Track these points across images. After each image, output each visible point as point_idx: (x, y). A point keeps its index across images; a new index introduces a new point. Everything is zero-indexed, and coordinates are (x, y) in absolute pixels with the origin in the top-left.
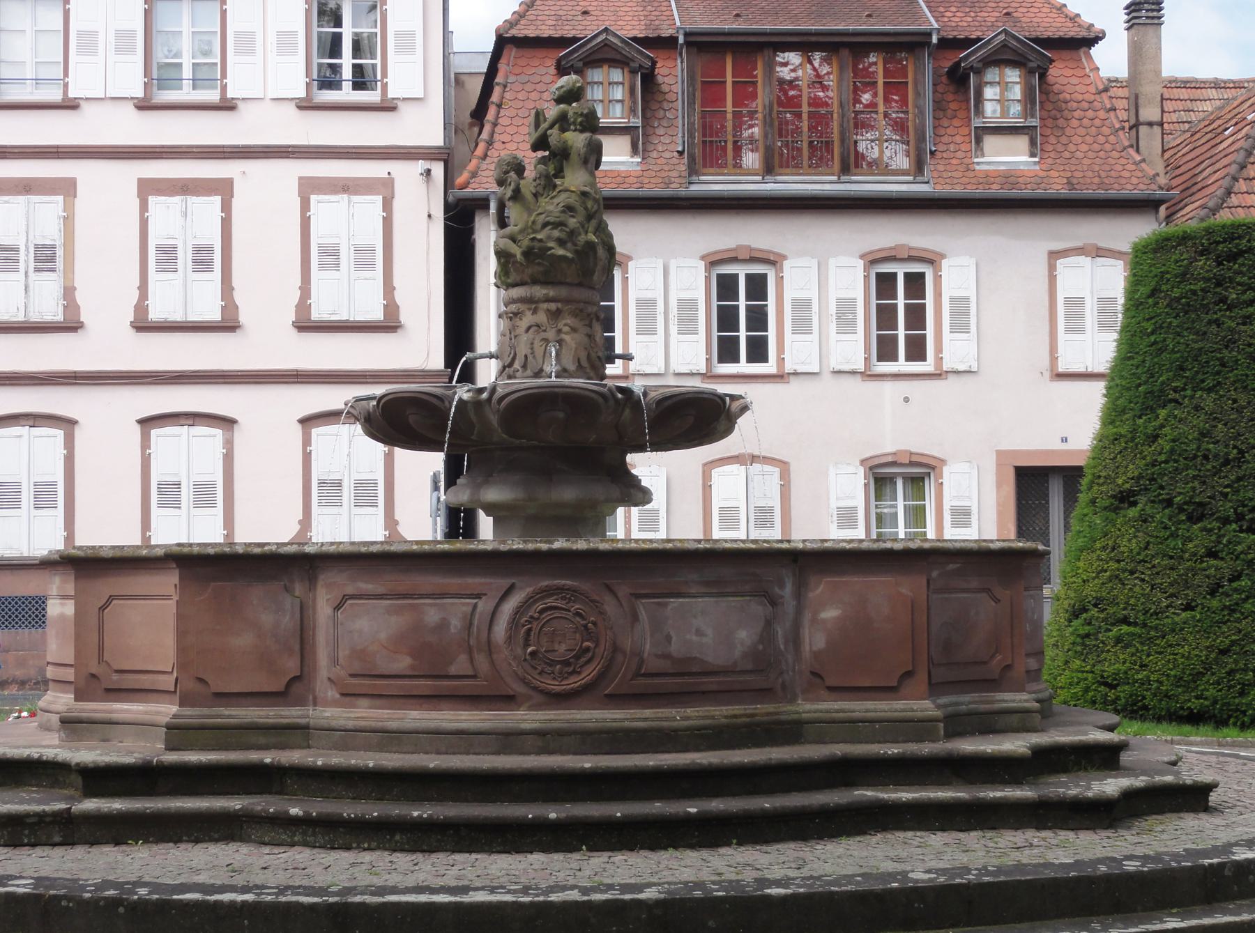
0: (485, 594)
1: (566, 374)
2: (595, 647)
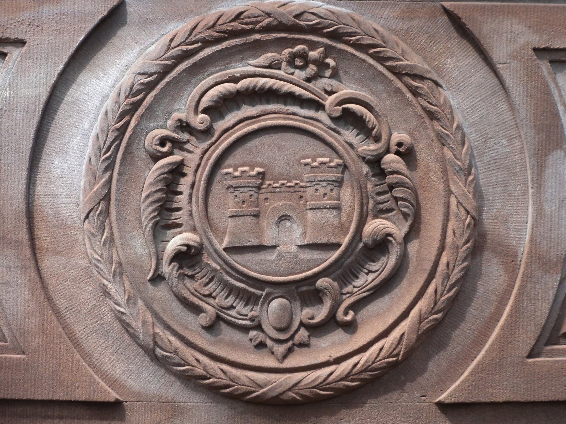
0: (20, 43)
1: (158, 340)
2: (407, 238)
